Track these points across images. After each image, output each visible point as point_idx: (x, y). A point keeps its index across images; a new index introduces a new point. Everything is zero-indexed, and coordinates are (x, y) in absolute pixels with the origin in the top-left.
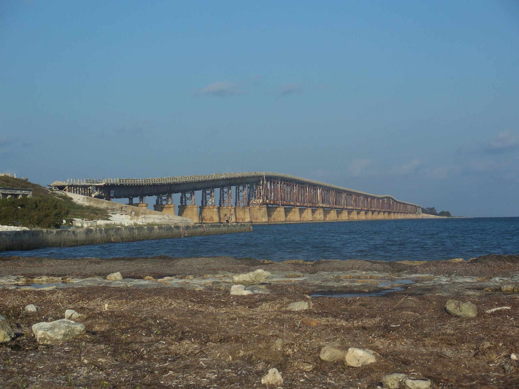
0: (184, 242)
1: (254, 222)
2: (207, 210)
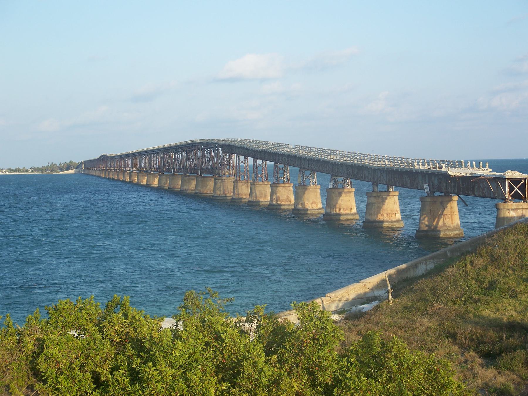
1: (229, 197)
2: (282, 189)
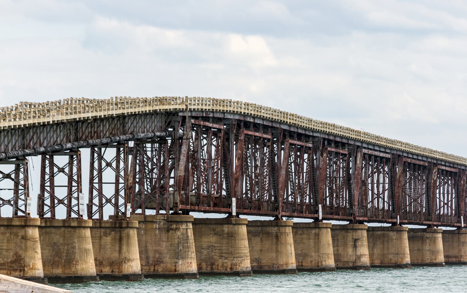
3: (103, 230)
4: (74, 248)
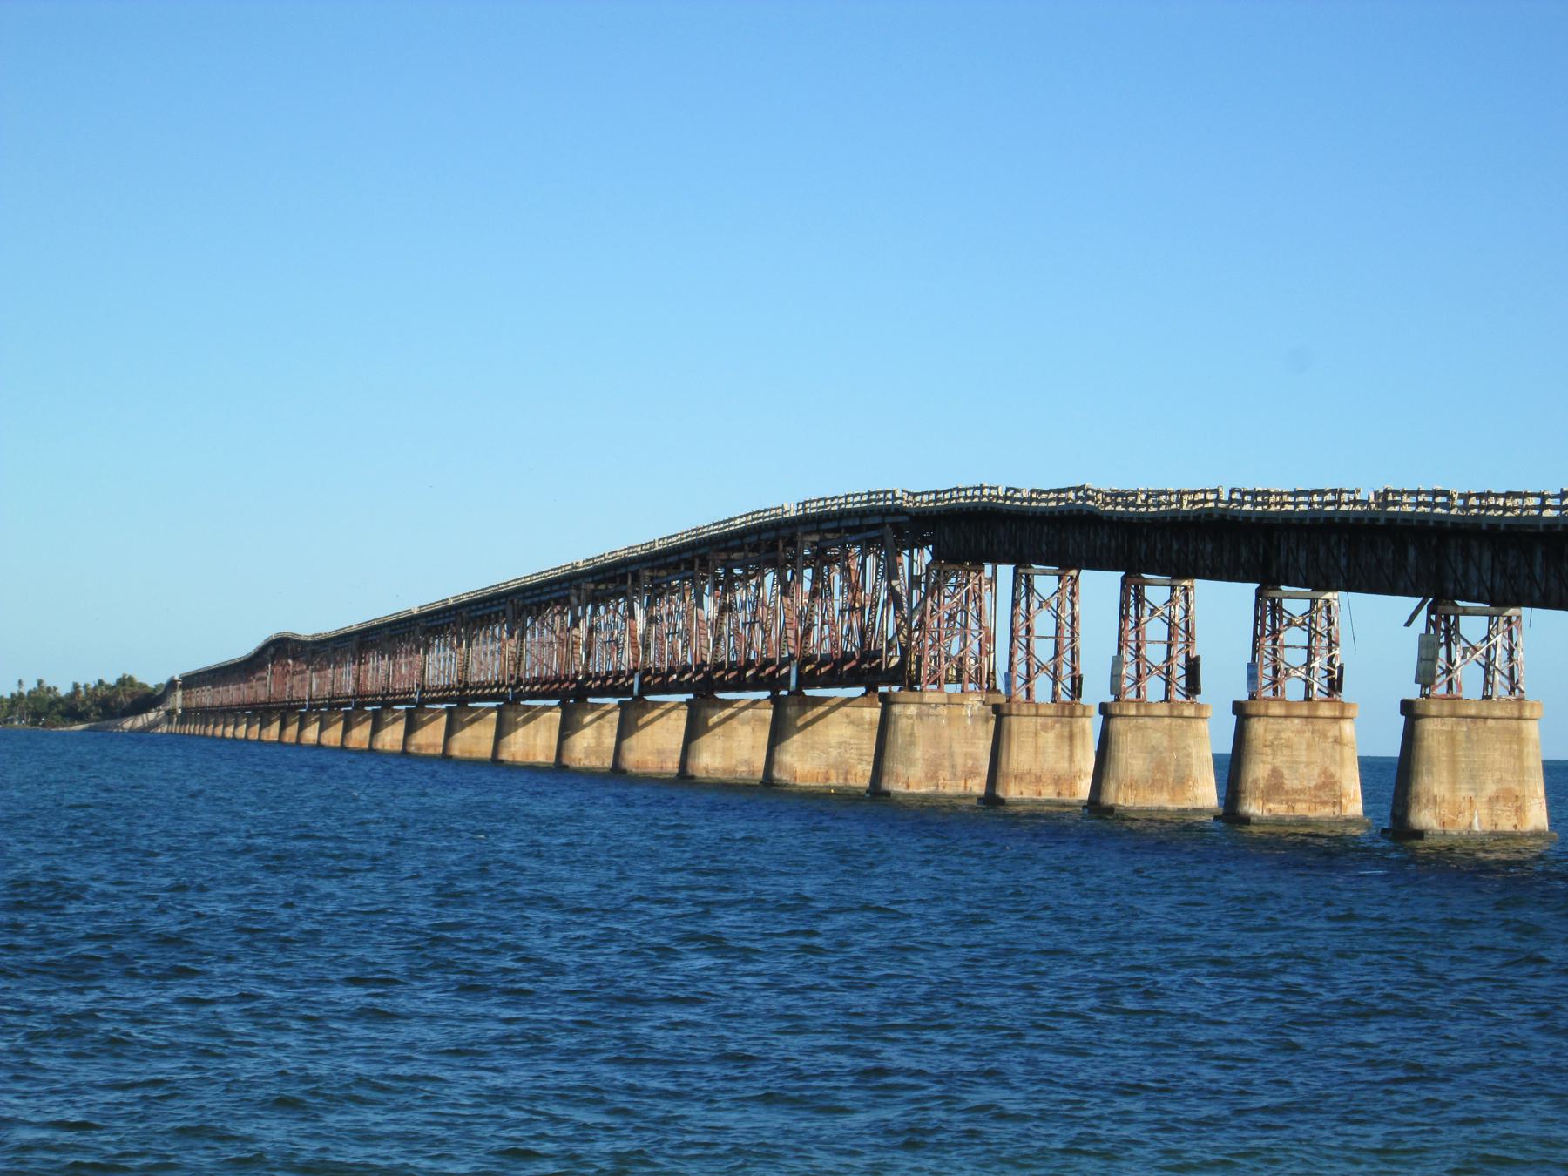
0: (326, 1046)
2: (1300, 732)
3: (1040, 720)
4: (1189, 755)
